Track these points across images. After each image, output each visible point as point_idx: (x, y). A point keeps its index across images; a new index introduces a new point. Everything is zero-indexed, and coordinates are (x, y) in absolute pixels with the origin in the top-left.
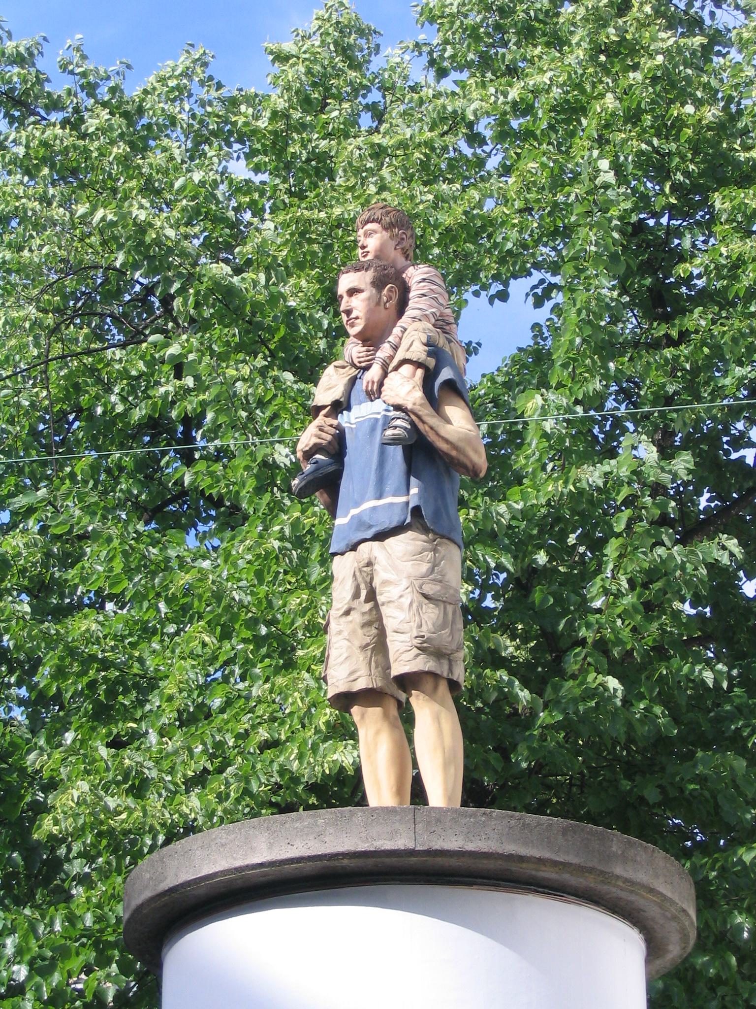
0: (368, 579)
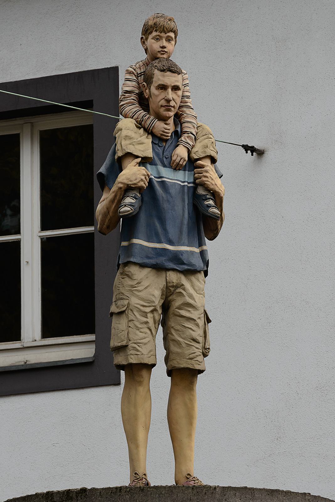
0: (169, 294)
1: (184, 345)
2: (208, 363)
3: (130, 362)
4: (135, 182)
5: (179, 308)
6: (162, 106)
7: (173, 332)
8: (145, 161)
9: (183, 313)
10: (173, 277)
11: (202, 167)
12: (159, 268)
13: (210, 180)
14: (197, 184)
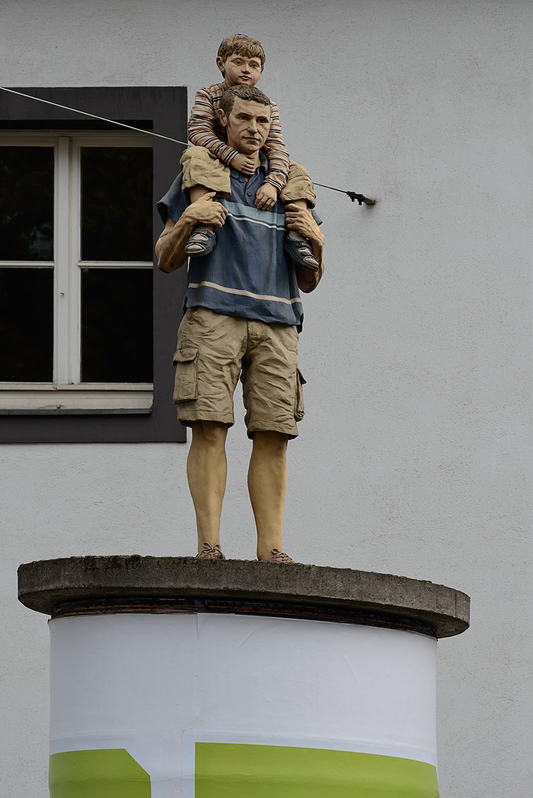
1: (270, 406)
2: (300, 428)
3: (199, 418)
4: (208, 218)
5: (264, 364)
6: (243, 137)
7: (256, 390)
8: (220, 196)
9: (269, 369)
10: (257, 329)
11: (296, 210)
12: (238, 317)
13: (306, 226)
14: (288, 229)
